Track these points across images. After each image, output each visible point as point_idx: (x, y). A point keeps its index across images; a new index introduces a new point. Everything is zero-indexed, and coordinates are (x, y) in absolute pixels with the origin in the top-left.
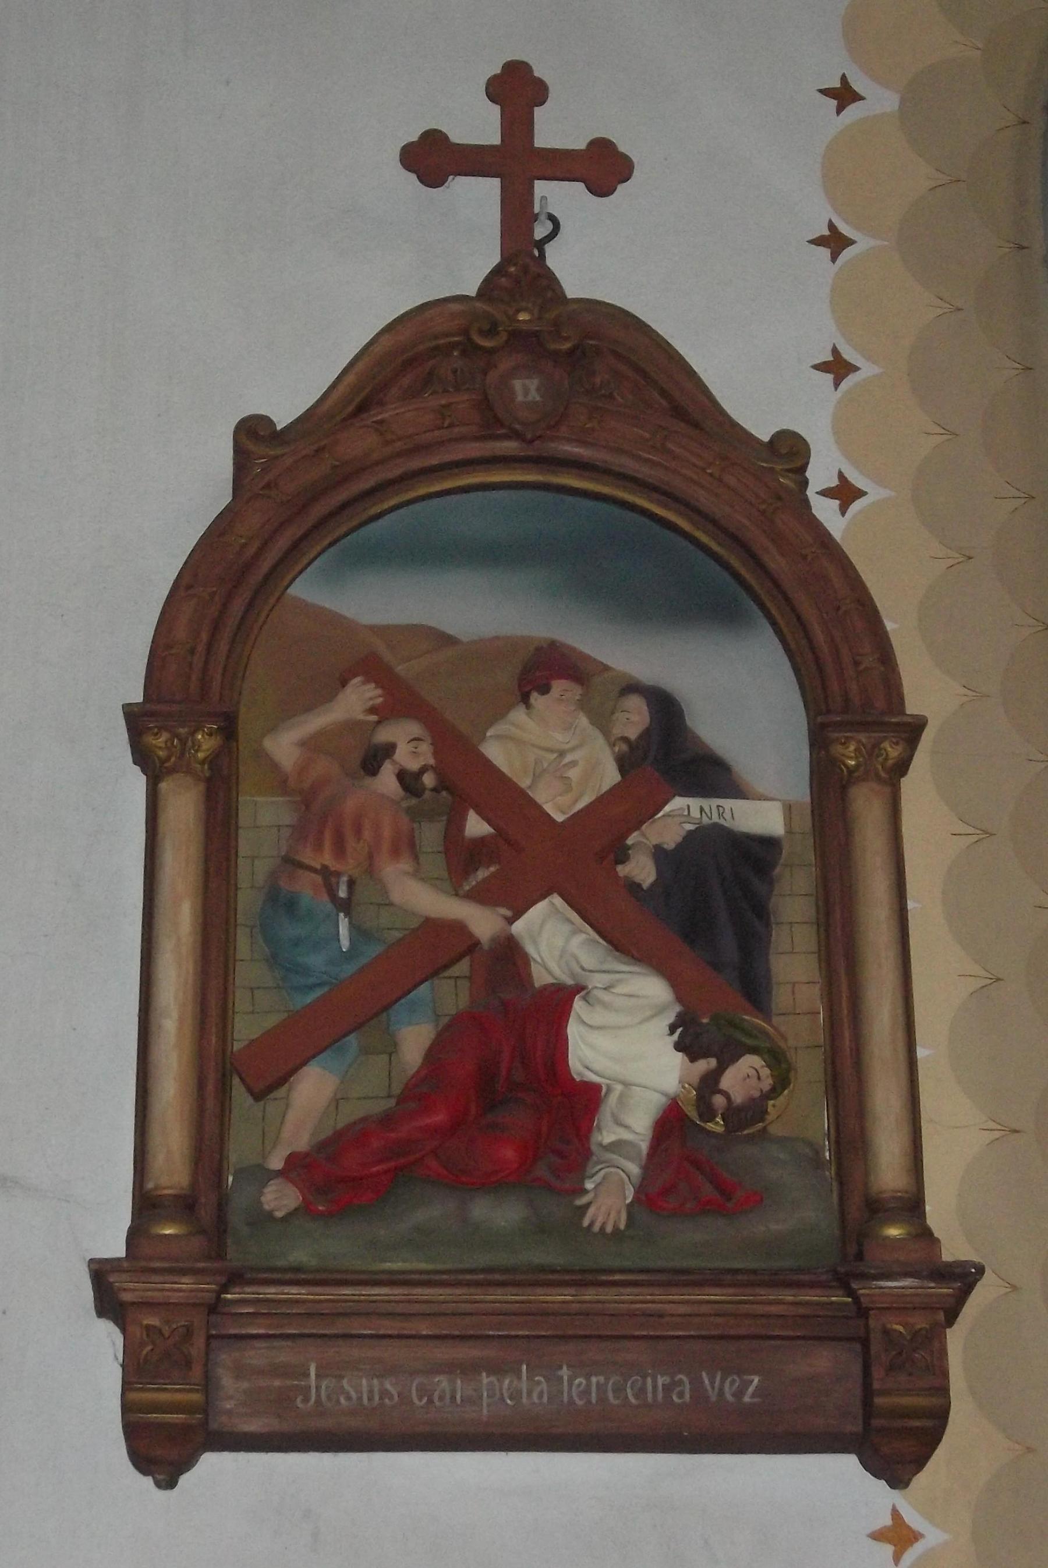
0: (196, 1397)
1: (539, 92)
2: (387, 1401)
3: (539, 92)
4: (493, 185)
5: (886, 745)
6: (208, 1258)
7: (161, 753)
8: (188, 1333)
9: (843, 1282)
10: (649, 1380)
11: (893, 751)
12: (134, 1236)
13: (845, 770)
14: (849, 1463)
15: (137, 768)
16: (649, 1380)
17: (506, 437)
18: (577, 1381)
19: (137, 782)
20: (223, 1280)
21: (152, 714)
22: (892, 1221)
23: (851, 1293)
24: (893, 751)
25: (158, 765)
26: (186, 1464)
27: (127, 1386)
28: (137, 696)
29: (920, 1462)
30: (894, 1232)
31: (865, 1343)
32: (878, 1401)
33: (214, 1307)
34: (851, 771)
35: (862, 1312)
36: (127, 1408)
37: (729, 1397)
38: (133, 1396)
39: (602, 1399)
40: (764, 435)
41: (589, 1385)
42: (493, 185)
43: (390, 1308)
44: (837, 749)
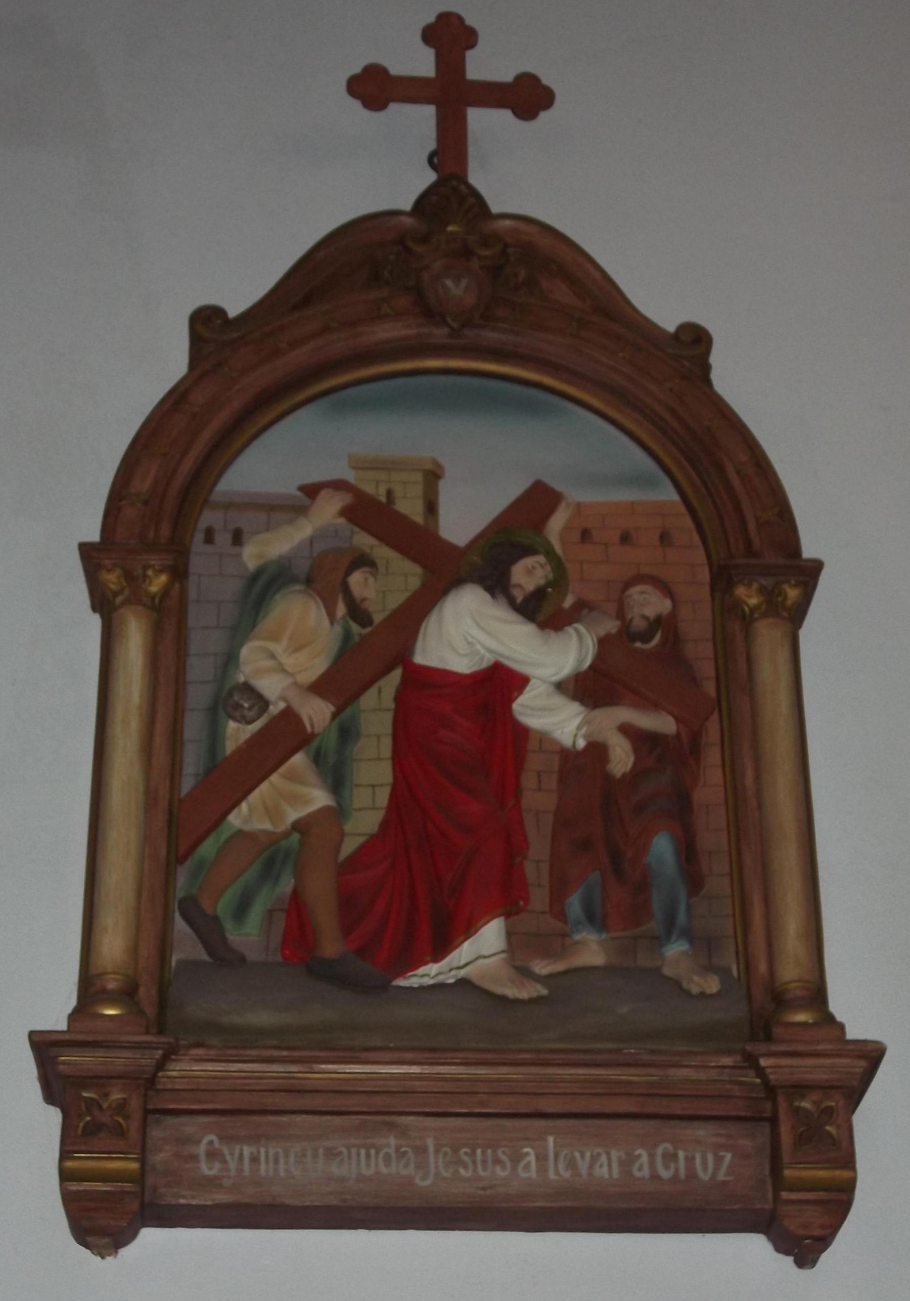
0: (135, 1166)
4: (428, 112)
7: (113, 587)
11: (793, 594)
15: (839, 1018)
19: (95, 622)
23: (761, 1072)
24: (793, 594)
28: (94, 536)
29: (824, 1241)
31: (774, 1121)
32: (787, 1173)
34: (752, 610)
39: (692, 1175)
42: (428, 112)
44: (740, 591)
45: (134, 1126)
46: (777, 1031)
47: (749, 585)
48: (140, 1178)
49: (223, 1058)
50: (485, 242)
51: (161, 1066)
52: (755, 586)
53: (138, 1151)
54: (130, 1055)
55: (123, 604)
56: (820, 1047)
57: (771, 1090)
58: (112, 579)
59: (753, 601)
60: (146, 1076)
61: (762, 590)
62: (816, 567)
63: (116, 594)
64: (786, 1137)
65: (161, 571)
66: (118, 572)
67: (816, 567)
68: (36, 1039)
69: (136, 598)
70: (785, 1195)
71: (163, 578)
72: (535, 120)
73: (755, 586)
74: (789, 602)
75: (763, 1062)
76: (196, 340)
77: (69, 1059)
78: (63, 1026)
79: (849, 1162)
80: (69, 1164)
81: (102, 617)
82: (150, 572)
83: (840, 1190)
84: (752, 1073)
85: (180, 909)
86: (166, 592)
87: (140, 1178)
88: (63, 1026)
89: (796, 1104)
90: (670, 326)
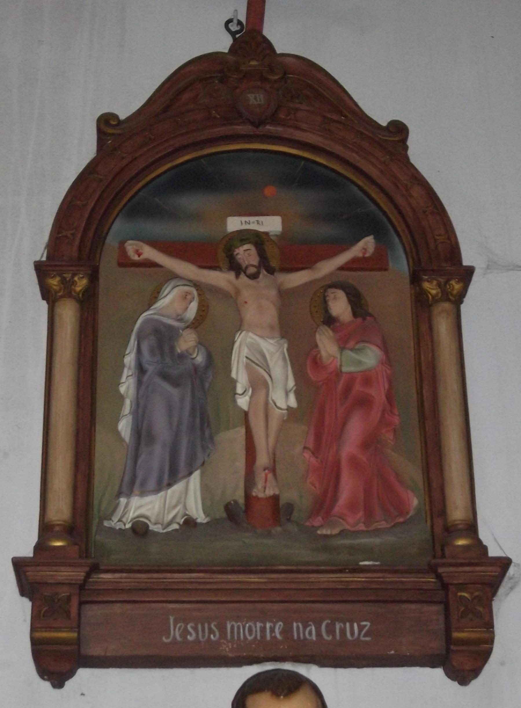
2: (212, 636)
5: (453, 282)
6: (80, 557)
7: (55, 287)
8: (69, 599)
9: (432, 569)
10: (348, 625)
11: (457, 286)
12: (39, 548)
14: (439, 672)
15: (485, 543)
16: (348, 625)
17: (243, 123)
18: (179, 625)
19: (44, 306)
20: (87, 569)
21: (50, 266)
22: (461, 537)
23: (439, 577)
24: (457, 286)
25: (54, 294)
26: (70, 674)
27: (33, 629)
29: (476, 672)
30: (461, 542)
33: (82, 587)
34: (433, 297)
35: (445, 586)
36: (35, 643)
37: (178, 638)
38: (38, 635)
40: (384, 123)
41: (265, 627)
43: (181, 586)
44: (426, 285)
46: (447, 552)
48: (78, 642)
49: (215, 568)
52: (435, 282)
54: (169, 166)
56: (252, 568)
58: (54, 282)
59: (434, 292)
60: (79, 582)
61: (439, 285)
62: (470, 272)
63: (56, 292)
66: (58, 279)
67: (470, 272)
69: (69, 294)
70: (452, 647)
71: (85, 281)
73: (435, 282)
74: (455, 292)
77: (32, 574)
78: (31, 555)
81: (48, 303)
82: (76, 279)
83: (479, 642)
84: (433, 576)
85: (244, 28)
87: (78, 642)
88: (31, 555)
89: (459, 594)
90: (384, 123)
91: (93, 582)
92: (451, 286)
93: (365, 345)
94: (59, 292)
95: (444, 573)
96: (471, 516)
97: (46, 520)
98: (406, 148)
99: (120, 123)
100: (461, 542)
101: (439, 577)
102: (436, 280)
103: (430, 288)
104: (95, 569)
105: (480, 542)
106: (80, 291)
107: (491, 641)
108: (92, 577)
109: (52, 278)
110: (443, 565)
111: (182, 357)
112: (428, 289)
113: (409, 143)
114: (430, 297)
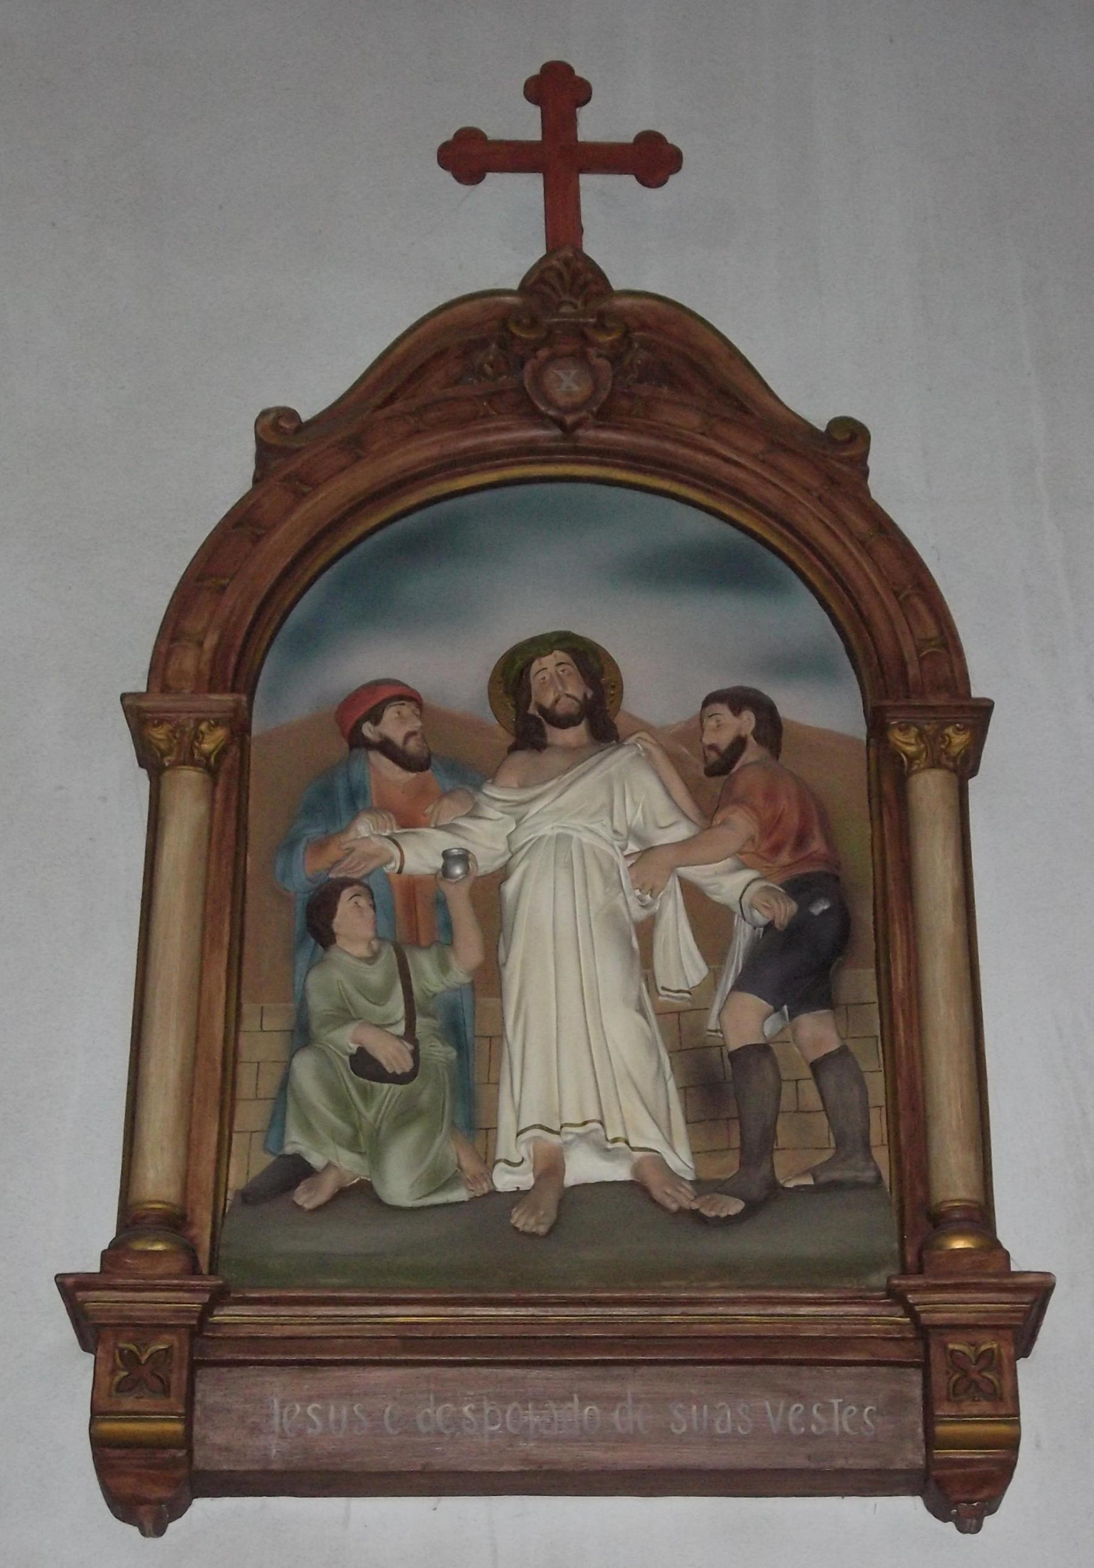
0: (179, 1427)
1: (582, 92)
3: (582, 92)
9: (895, 1296)
12: (111, 1256)
13: (905, 759)
15: (1006, 1246)
19: (142, 780)
20: (206, 1297)
22: (961, 1233)
23: (910, 1310)
24: (959, 740)
26: (177, 1510)
27: (97, 1413)
28: (139, 684)
30: (959, 1244)
31: (925, 1367)
34: (911, 759)
36: (100, 1444)
38: (107, 1427)
44: (897, 737)
45: (178, 1378)
47: (904, 730)
50: (601, 327)
51: (208, 1309)
52: (914, 731)
53: (181, 1411)
55: (174, 765)
57: (923, 1332)
59: (911, 749)
62: (985, 709)
64: (940, 1380)
65: (217, 725)
67: (985, 709)
68: (128, 702)
71: (220, 733)
72: (661, 188)
73: (914, 731)
75: (911, 1298)
76: (265, 453)
78: (96, 1268)
79: (1013, 1417)
80: (107, 1427)
82: (203, 727)
86: (222, 752)
87: (187, 1441)
88: (96, 1268)
89: (951, 1346)
91: (218, 1324)
92: (947, 738)
93: (908, 1174)
94: (170, 751)
95: (917, 1304)
96: (976, 1196)
97: (134, 1197)
98: (866, 473)
99: (302, 427)
100: (959, 1244)
101: (910, 1310)
102: (915, 725)
103: (903, 742)
104: (220, 1297)
105: (998, 1245)
106: (211, 753)
107: (1012, 1444)
108: (215, 1313)
109: (155, 726)
110: (915, 1290)
111: (965, 728)
112: (899, 744)
113: (872, 462)
114: (905, 759)
